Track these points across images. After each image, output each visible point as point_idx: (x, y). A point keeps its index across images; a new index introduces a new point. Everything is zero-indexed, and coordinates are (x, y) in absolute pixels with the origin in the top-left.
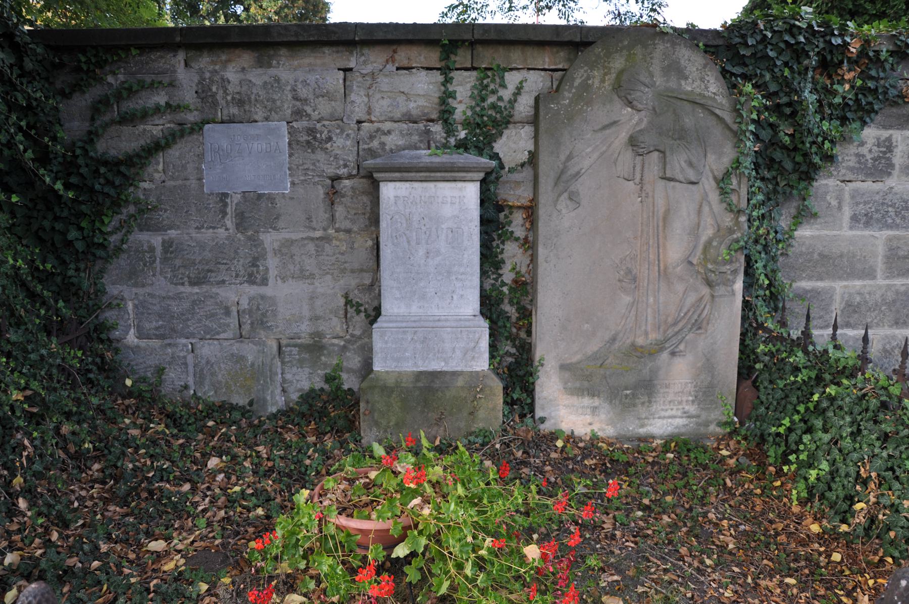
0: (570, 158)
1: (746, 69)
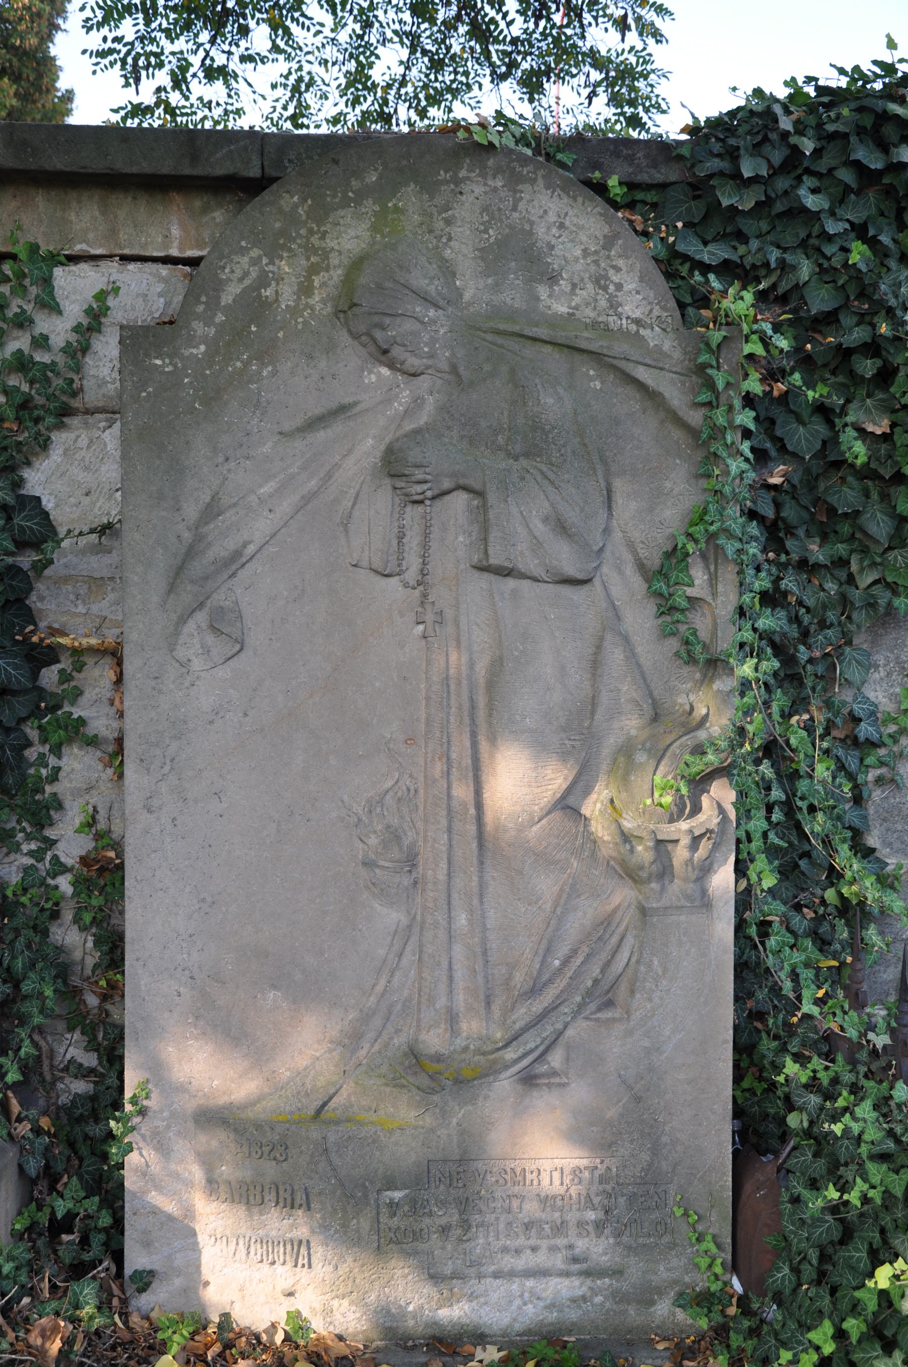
0: (211, 512)
1: (742, 249)
